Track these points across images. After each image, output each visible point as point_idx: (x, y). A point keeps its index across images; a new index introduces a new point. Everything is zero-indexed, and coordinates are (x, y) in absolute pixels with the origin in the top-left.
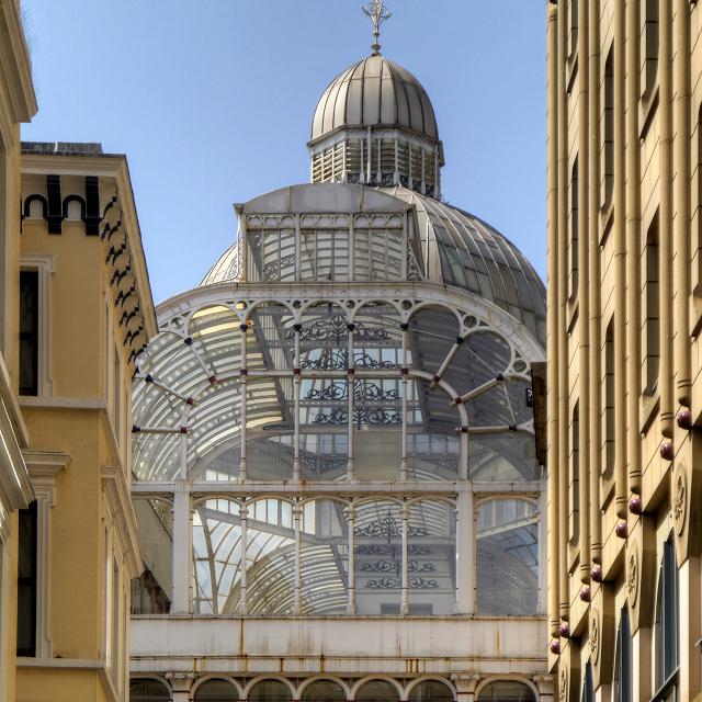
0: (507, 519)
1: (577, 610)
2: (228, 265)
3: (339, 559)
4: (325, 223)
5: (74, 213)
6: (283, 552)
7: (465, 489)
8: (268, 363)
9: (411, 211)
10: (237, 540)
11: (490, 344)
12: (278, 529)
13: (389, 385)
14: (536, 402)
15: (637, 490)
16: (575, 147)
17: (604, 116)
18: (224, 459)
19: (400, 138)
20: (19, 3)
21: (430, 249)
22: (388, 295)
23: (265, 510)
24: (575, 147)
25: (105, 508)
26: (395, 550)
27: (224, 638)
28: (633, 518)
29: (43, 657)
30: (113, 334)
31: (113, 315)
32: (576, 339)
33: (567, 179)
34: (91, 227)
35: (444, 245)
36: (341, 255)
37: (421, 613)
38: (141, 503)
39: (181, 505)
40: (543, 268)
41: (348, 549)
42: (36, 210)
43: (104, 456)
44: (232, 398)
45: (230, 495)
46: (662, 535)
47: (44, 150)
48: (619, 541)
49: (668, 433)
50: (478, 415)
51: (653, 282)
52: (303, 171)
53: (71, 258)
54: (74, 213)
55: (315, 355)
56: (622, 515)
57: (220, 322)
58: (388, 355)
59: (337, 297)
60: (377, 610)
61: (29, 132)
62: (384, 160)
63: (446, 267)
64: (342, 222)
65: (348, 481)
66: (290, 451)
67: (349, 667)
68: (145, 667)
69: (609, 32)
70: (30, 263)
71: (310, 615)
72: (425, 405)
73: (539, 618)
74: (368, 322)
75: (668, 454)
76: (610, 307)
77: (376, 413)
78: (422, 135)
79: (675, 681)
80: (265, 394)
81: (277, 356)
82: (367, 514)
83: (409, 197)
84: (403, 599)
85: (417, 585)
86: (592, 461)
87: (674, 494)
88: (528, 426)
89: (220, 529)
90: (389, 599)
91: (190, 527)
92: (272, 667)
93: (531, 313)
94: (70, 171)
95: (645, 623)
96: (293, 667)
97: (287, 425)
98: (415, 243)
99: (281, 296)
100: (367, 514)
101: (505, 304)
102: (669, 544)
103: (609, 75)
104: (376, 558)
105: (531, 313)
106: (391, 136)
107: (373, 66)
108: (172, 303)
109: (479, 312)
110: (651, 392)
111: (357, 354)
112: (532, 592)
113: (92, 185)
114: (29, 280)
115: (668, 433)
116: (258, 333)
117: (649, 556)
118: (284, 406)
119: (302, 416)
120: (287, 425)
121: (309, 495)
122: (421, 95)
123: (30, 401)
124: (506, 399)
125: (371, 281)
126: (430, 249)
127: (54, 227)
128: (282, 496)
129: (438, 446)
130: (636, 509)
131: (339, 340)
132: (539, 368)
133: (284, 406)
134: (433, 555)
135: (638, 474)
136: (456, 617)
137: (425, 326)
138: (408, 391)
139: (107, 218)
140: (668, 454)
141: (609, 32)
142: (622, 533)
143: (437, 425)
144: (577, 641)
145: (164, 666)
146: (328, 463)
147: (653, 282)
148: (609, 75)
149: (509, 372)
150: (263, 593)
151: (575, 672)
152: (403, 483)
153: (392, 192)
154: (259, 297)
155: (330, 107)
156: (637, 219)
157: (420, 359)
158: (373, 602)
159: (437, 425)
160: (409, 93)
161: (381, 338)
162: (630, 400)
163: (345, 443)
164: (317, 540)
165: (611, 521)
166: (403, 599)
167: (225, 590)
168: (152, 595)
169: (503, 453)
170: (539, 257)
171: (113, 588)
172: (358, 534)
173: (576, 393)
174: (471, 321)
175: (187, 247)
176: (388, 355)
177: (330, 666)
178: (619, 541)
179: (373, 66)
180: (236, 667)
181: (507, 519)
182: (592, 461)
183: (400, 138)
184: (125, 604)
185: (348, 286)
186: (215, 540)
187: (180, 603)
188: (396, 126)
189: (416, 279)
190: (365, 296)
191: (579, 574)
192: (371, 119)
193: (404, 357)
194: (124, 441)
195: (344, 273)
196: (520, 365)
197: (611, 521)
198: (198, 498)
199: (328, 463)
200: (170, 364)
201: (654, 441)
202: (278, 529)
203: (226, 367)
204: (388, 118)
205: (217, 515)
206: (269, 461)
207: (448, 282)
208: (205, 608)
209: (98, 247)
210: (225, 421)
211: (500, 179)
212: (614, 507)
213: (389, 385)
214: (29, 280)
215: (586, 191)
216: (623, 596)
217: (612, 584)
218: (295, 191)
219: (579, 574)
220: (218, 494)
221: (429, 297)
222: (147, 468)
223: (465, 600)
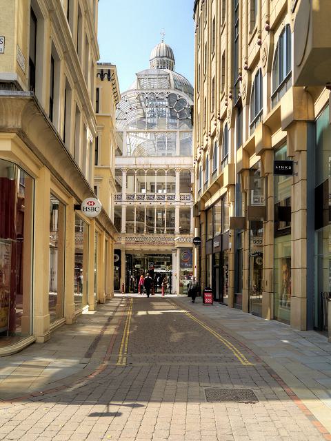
0: (187, 136)
1: (199, 155)
2: (134, 85)
3: (154, 144)
4: (153, 77)
5: (106, 76)
6: (143, 143)
7: (178, 130)
8: (141, 105)
9: (169, 74)
10: (133, 141)
11: (183, 101)
12: (143, 138)
13: (164, 109)
14: (192, 113)
15: (219, 114)
16: (199, 62)
17: (205, 56)
18: (133, 124)
19: (167, 59)
20: (87, 15)
21: (172, 81)
22: (164, 91)
23: (141, 135)
24: (199, 62)
25: (111, 135)
26: (165, 142)
27: (132, 161)
28: (209, 137)
29: (99, 166)
30: (113, 100)
31: (113, 97)
32: (199, 101)
33: (198, 69)
34: (109, 79)
35: (175, 81)
36: (156, 83)
37: (170, 155)
38: (117, 134)
39: (125, 134)
40: (194, 87)
41: (156, 142)
42: (99, 75)
43: (111, 126)
44: (134, 112)
45: (134, 132)
46: (214, 141)
47: (101, 64)
48: (207, 142)
49: (227, 100)
50: (181, 115)
51: (223, 75)
52: (148, 67)
53: (105, 86)
54: (106, 76)
55: (150, 103)
56: (216, 120)
57: (132, 97)
58: (164, 103)
59: (154, 92)
60: (161, 155)
61: (99, 61)
62: (164, 63)
63: (175, 85)
64: (156, 77)
65: (156, 129)
66: (145, 122)
67: (156, 167)
68: (118, 167)
69: (206, 40)
70: (98, 87)
71: (148, 156)
72: (171, 113)
73: (192, 157)
74: (161, 97)
75: (216, 125)
76: (205, 95)
77: (161, 115)
78: (171, 58)
79: (216, 170)
80: (141, 111)
81: (143, 103)
82: (160, 135)
83: (168, 71)
84: (166, 152)
85: (169, 149)
86: (202, 125)
87: (217, 133)
88: (190, 118)
89: (132, 138)
90: (163, 152)
91: (126, 138)
92: (141, 167)
93: (191, 95)
94: (105, 68)
95: (211, 158)
96: (145, 167)
97: (145, 118)
98: (169, 81)
99: (144, 92)
100: (160, 135)
101: (186, 92)
102: (226, 126)
103: (214, 23)
104: (161, 144)
105: (191, 95)
106: (165, 59)
107: (162, 44)
108: (123, 94)
109: (181, 95)
110: (213, 112)
111: (158, 103)
112: (190, 150)
113: (109, 71)
114: (98, 90)
115: (227, 100)
116: (140, 99)
117: (212, 145)
118: (144, 114)
119: (147, 115)
120: (145, 118)
121: (149, 132)
122: (171, 50)
123: (97, 114)
124: (186, 112)
125: (161, 89)
126: (172, 81)
127: (102, 79)
128: (144, 132)
129: (173, 121)
130: (219, 118)
131: (155, 100)
132: (192, 106)
133: (144, 114)
134: (172, 143)
135: (210, 128)
136: (176, 157)
137: (171, 96)
138: (168, 110)
139: (112, 77)
140: (216, 125)
141: (206, 40)
142: (207, 140)
143: (173, 117)
144: (199, 161)
145: (121, 166)
146: (153, 125)
147: (223, 75)
148: (214, 23)
149: (187, 107)
150: (140, 152)
151: (198, 168)
152: (166, 129)
153: (165, 70)
154: (140, 92)
155: (154, 53)
156: (211, 77)
157: (170, 103)
158: (160, 153)
159: (173, 117)
160: (169, 50)
161: (162, 100)
162: (218, 103)
163: (155, 121)
164: (148, 141)
165: (205, 138)
166: (166, 152)
167: (132, 151)
168: (119, 152)
169: (185, 123)
170: (193, 83)
171: (112, 151)
172: (158, 139)
173: (199, 112)
174: (180, 96)
175: (126, 82)
176: (164, 103)
177: (152, 167)
178: (207, 142)
179: (162, 44)
180: (135, 167)
181: (187, 136)
182: (202, 125)
183: (167, 59)
184: (114, 154)
185: (156, 89)
186: (131, 140)
187: (124, 154)
188: (166, 56)
189: (169, 88)
190: (159, 91)
191: (199, 148)
192: (161, 55)
193: (167, 103)
194: (114, 121)
195: (156, 87)
196: (189, 105)
197: (205, 138)
198: (128, 132)
199: (153, 125)
200: (122, 104)
201: (213, 122)
202: (143, 138)
203: (134, 106)
204: (165, 55)
205: (131, 135)
206: (144, 124)
207: (176, 88)
208: (129, 155)
209: (110, 83)
210: (135, 116)
211: (186, 69)
212: (206, 135)
213: (164, 109)
214: (98, 90)
215: (201, 71)
216: (207, 152)
217: (205, 150)
218: (147, 70)
219: (199, 148)
220: (131, 132)
221: (172, 92)
222: (119, 126)
223: (178, 153)
